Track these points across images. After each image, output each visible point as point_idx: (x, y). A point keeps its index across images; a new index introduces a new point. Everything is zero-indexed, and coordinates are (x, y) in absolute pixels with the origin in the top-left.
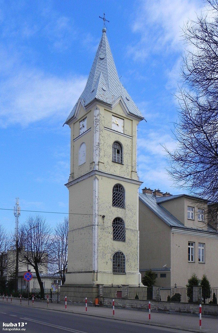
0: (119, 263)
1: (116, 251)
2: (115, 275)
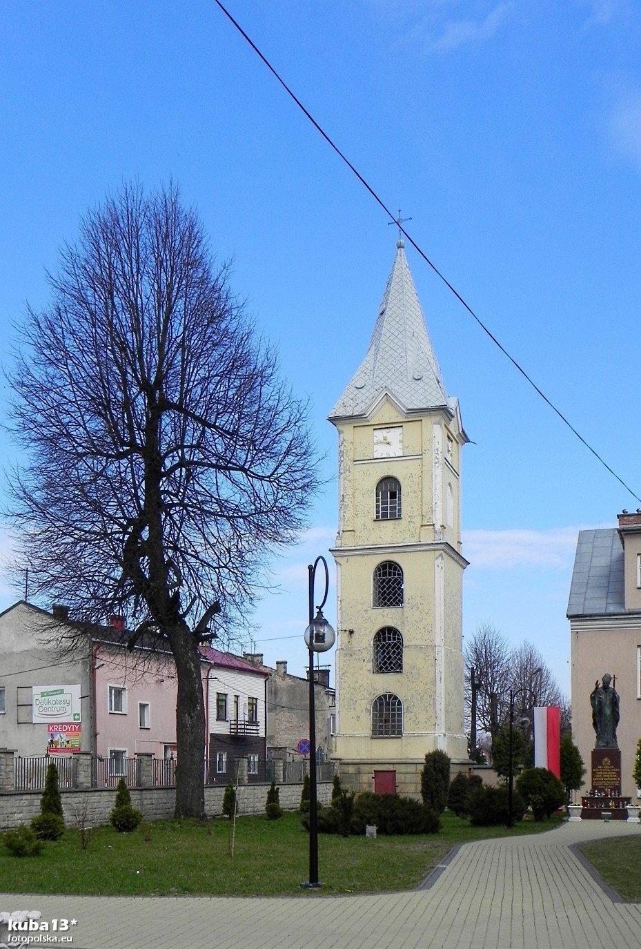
0: (387, 718)
1: (381, 692)
2: (375, 740)
